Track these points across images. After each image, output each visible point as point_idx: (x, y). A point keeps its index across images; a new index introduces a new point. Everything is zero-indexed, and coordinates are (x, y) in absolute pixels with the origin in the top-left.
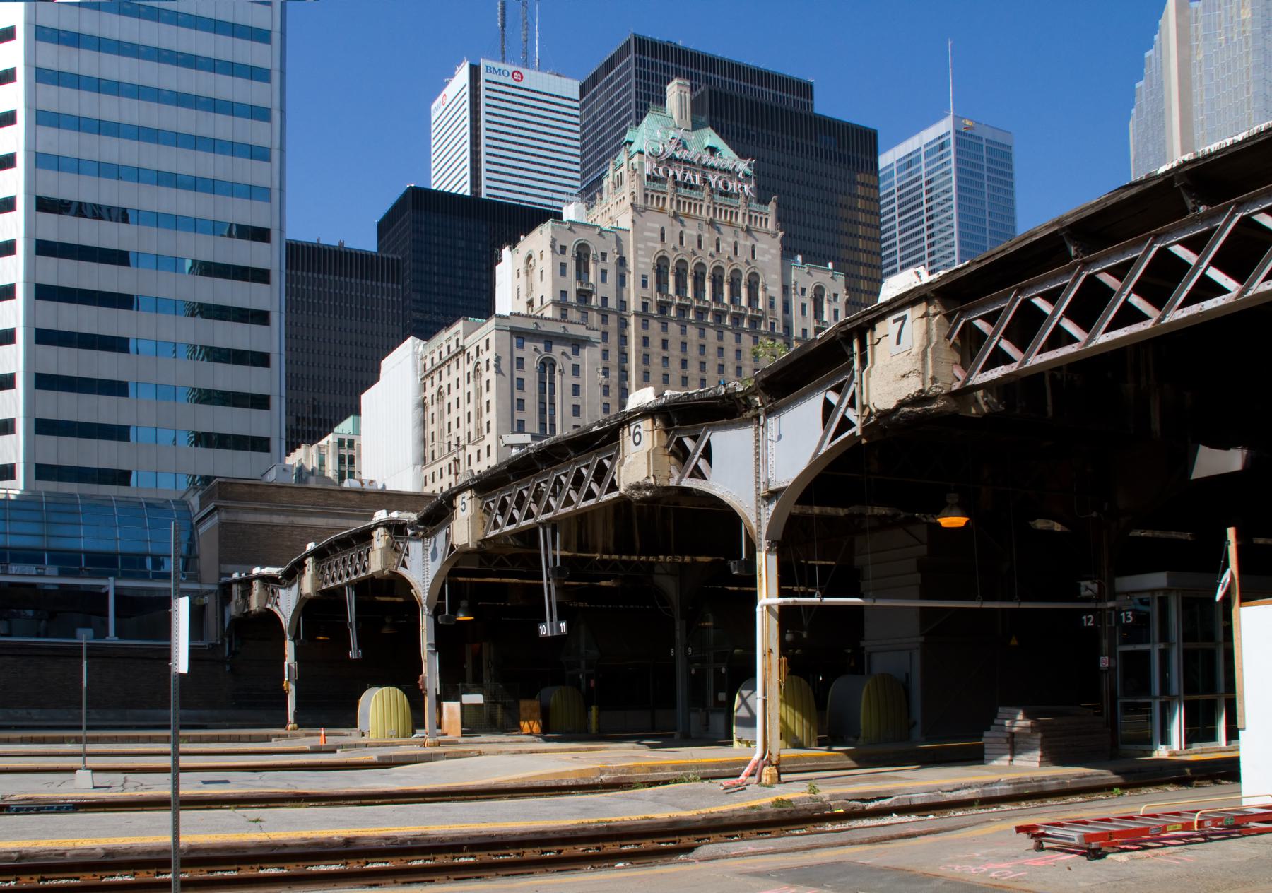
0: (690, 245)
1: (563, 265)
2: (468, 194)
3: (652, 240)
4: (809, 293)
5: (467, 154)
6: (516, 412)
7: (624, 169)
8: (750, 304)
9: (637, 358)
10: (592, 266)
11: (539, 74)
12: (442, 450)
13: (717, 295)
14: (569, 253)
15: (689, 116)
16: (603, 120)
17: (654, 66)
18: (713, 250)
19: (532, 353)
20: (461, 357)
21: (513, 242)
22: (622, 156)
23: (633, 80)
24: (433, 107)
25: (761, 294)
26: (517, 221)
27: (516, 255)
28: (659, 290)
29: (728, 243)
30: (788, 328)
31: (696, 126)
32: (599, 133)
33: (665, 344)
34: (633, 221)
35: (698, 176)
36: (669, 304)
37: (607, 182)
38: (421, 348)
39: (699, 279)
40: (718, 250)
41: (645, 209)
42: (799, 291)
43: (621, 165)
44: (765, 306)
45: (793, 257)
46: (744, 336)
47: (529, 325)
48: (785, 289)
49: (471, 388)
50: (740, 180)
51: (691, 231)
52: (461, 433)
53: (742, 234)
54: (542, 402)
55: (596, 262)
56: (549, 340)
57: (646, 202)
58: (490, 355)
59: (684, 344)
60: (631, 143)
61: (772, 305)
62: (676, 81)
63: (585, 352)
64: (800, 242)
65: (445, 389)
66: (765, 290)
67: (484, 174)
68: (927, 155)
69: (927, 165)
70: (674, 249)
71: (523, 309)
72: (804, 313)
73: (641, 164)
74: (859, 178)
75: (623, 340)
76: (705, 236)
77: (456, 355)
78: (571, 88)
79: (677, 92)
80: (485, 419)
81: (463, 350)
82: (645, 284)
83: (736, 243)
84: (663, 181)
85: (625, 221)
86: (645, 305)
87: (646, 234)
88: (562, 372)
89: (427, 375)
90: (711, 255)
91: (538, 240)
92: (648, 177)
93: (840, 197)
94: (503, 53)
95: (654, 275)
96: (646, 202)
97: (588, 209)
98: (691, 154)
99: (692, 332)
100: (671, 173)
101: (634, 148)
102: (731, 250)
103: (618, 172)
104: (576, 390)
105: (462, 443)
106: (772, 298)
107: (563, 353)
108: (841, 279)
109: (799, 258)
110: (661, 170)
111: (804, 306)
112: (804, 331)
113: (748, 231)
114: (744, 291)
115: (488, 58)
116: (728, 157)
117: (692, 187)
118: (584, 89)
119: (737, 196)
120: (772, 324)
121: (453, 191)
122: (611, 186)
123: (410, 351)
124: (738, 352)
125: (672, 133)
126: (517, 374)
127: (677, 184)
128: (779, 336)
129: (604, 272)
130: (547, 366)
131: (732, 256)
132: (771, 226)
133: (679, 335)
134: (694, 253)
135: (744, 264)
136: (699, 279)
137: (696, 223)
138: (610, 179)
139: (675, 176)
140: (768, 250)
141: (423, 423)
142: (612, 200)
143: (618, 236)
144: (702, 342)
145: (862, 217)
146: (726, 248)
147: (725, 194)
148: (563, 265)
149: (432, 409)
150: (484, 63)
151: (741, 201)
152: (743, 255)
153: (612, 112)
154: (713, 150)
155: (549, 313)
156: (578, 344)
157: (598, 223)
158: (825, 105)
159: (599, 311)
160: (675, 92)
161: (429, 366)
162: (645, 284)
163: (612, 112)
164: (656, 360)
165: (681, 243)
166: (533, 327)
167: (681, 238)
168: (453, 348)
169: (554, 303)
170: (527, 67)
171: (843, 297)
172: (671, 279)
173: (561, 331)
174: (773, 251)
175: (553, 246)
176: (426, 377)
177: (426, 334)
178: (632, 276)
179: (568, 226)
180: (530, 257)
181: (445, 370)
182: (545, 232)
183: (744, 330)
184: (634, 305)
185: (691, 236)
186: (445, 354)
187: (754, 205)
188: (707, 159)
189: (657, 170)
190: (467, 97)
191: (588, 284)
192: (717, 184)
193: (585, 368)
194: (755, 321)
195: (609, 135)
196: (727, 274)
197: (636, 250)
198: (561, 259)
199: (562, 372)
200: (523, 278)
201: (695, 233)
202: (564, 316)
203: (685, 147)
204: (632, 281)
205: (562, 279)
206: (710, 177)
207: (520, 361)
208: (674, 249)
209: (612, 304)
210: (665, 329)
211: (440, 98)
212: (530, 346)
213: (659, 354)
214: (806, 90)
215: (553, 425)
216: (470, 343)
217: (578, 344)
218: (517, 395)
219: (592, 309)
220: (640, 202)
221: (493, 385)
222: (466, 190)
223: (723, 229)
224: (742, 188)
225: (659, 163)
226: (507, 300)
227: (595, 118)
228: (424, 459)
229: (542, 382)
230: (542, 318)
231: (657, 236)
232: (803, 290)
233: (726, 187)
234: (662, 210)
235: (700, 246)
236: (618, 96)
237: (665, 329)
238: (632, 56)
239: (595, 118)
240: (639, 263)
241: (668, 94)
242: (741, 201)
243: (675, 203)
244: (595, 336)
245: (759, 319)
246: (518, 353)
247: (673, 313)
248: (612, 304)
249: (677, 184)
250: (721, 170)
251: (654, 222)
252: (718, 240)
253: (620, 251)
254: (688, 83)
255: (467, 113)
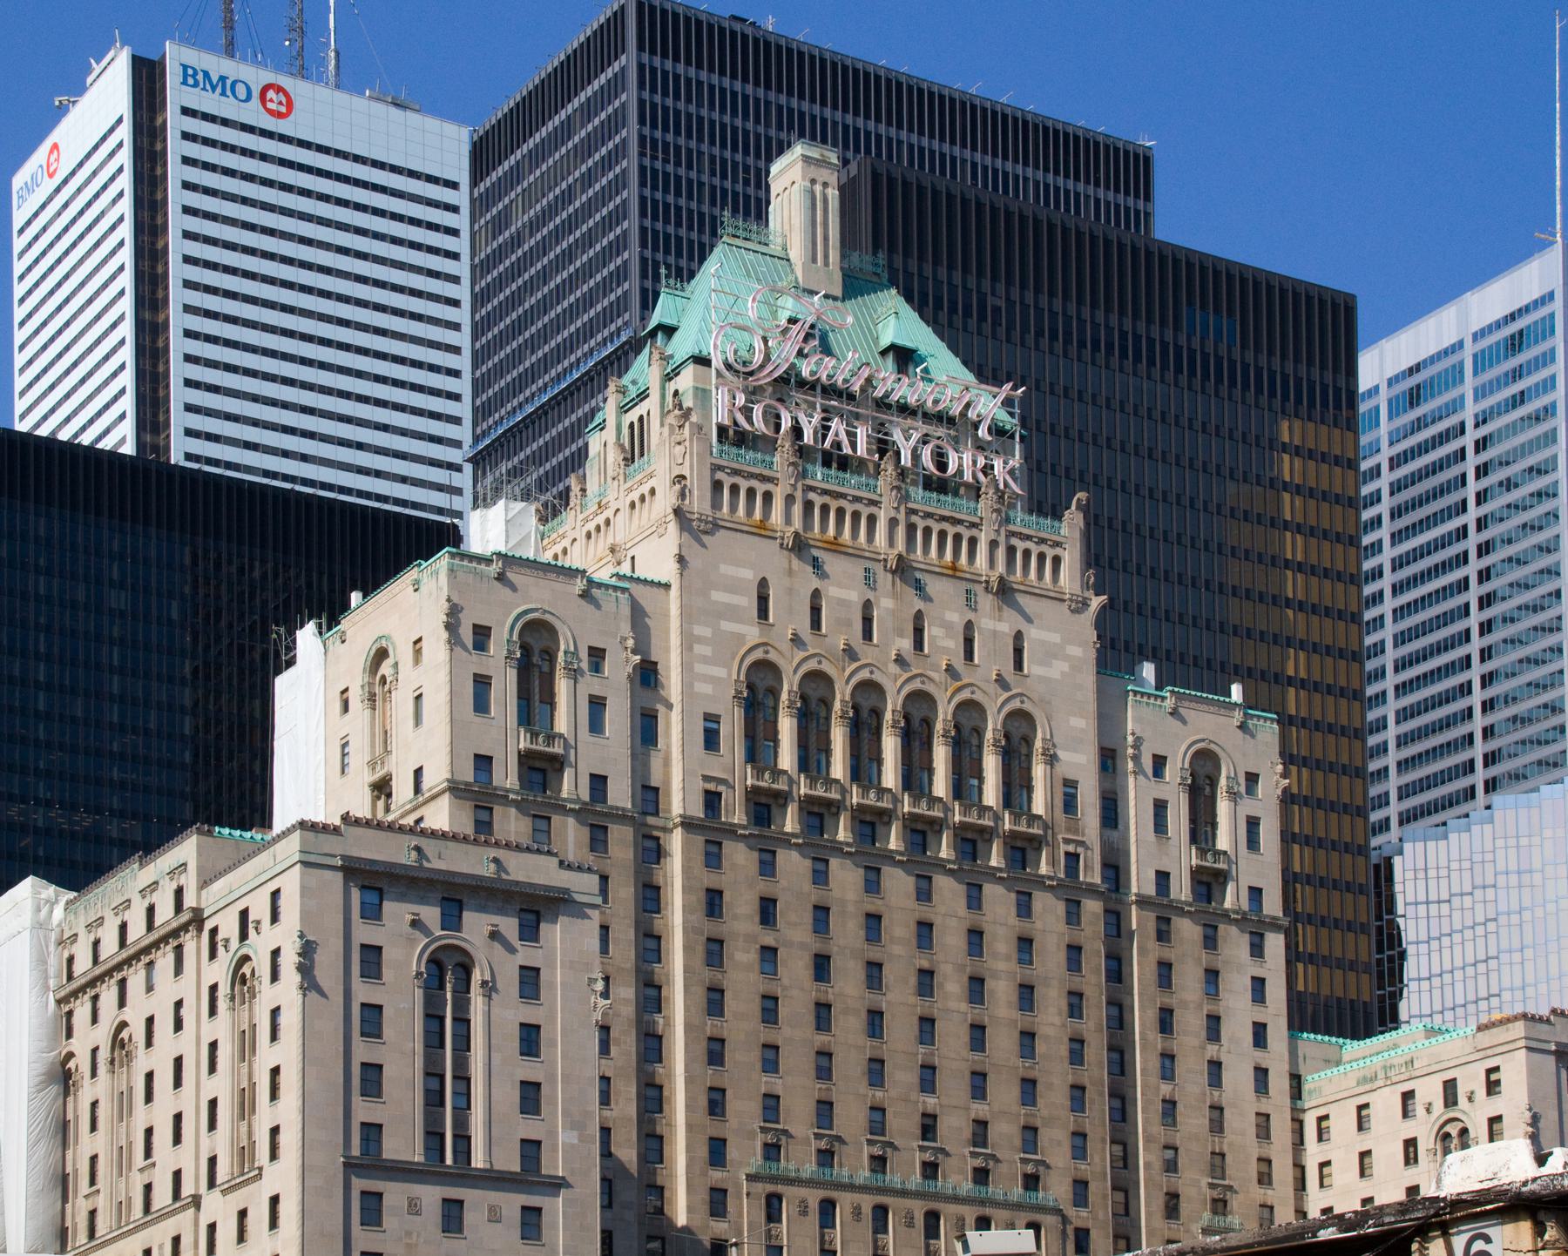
0: (839, 631)
1: (482, 683)
2: (128, 449)
3: (731, 613)
4: (1175, 771)
5: (127, 330)
6: (356, 1099)
7: (651, 405)
8: (1008, 800)
9: (687, 948)
10: (562, 687)
11: (342, 97)
12: (121, 1208)
13: (915, 774)
14: (499, 645)
15: (834, 255)
16: (543, 247)
17: (692, 90)
18: (906, 644)
19: (404, 932)
20: (189, 943)
21: (331, 612)
22: (644, 370)
23: (631, 131)
24: (18, 181)
25: (1039, 771)
26: (363, 546)
27: (335, 646)
28: (752, 756)
29: (947, 626)
30: (1115, 869)
31: (854, 286)
32: (530, 288)
33: (767, 910)
34: (681, 559)
35: (862, 433)
36: (782, 798)
37: (602, 444)
38: (59, 912)
39: (864, 728)
40: (918, 645)
41: (715, 526)
42: (1148, 763)
43: (643, 396)
44: (1051, 806)
45: (1132, 670)
46: (991, 891)
47: (399, 853)
48: (1109, 759)
49: (222, 1029)
50: (980, 447)
51: (843, 589)
52: (188, 1159)
53: (986, 602)
54: (433, 1073)
55: (574, 674)
56: (455, 896)
57: (716, 505)
58: (285, 935)
59: (822, 913)
60: (669, 331)
61: (1070, 804)
62: (798, 150)
63: (556, 932)
64: (1159, 622)
65: (137, 1030)
66: (1051, 759)
67: (178, 395)
68: (1482, 362)
69: (1480, 393)
70: (796, 640)
71: (362, 807)
72: (1160, 826)
73: (702, 394)
74: (1286, 431)
75: (650, 897)
76: (884, 605)
77: (175, 933)
78: (444, 146)
79: (802, 184)
80: (265, 1117)
81: (198, 919)
82: (711, 740)
83: (969, 626)
84: (766, 444)
85: (657, 557)
86: (712, 800)
87: (718, 596)
88: (489, 988)
89: (75, 992)
90: (900, 660)
91: (406, 611)
92: (722, 430)
93: (1231, 487)
94: (229, 25)
95: (739, 713)
96: (716, 505)
97: (543, 520)
98: (842, 368)
99: (846, 878)
100: (786, 423)
101: (681, 347)
102: (955, 645)
103: (633, 416)
104: (530, 1039)
105: (187, 1190)
106: (1070, 784)
107: (495, 935)
108: (1268, 731)
109: (1148, 671)
110: (758, 411)
111: (1160, 807)
112: (1163, 877)
113: (1004, 592)
114: (991, 764)
115: (184, 41)
116: (947, 377)
117: (844, 464)
118: (483, 156)
119: (975, 491)
120: (1073, 858)
121: (86, 439)
122: (613, 456)
123: (27, 919)
124: (976, 936)
125: (788, 306)
126: (364, 992)
127: (803, 452)
128: (1092, 890)
129: (597, 704)
130: (447, 970)
131: (959, 663)
132: (1070, 577)
133: (807, 886)
134: (850, 653)
135: (993, 688)
136: (864, 728)
137: (856, 569)
138: (609, 434)
139: (797, 431)
140: (1060, 647)
141: (63, 1131)
142: (617, 497)
143: (636, 599)
144: (874, 905)
145: (1293, 547)
146: (942, 640)
147: (939, 485)
148: (482, 683)
149: (87, 1091)
150: (175, 56)
151: (985, 506)
152: (991, 660)
153: (570, 225)
154: (904, 357)
155: (439, 816)
156: (535, 909)
157: (574, 560)
158: (1182, 218)
159: (581, 813)
160: (796, 182)
161: (83, 964)
162: (711, 740)
163: (570, 225)
164: (742, 956)
165: (816, 624)
166: (408, 859)
167: (816, 611)
168: (165, 913)
169: (455, 789)
170: (303, 73)
171: (1272, 783)
172: (787, 727)
173: (488, 871)
174: (1075, 651)
175: (451, 627)
176: (75, 994)
177: (77, 870)
178: (675, 716)
179: (495, 568)
180: (382, 654)
181: (136, 978)
182: (428, 584)
183: (991, 874)
184: (680, 800)
185: (842, 603)
186: (137, 931)
187: (1021, 519)
188: (887, 380)
189: (747, 412)
190: (125, 157)
191: (551, 737)
192: (916, 456)
193: (556, 978)
194: (1022, 850)
195: (559, 294)
196: (892, 705)
197: (688, 642)
198: (475, 663)
199: (489, 988)
200: (356, 716)
201: (854, 596)
202: (484, 826)
203: (826, 350)
204: (675, 730)
205: (478, 720)
206: (897, 436)
207: (372, 953)
208: (796, 640)
209: (620, 794)
210: (767, 867)
211: (40, 155)
212: (397, 912)
213: (750, 938)
214: (1131, 170)
215: (463, 1139)
216: (219, 902)
217: (535, 909)
218: (363, 1051)
219: (562, 809)
220: (699, 503)
221: (290, 1021)
222: (122, 439)
223: (934, 586)
224: (988, 469)
225: (753, 393)
226: (309, 772)
227: (517, 241)
228: (63, 1236)
229: (433, 1018)
230: (416, 830)
231: (749, 602)
232: (1159, 762)
233: (942, 466)
234: (762, 530)
235: (867, 634)
236: (588, 180)
237: (767, 867)
238: (628, 60)
239: (517, 241)
240: (696, 682)
241: (775, 188)
242: (985, 506)
243: (797, 509)
244: (583, 885)
245: (1036, 843)
246: (365, 933)
247: (790, 822)
248: (620, 794)
249: (803, 452)
250: (927, 417)
251: (741, 563)
252: (919, 616)
253: (641, 646)
254: (833, 158)
255: (126, 206)
